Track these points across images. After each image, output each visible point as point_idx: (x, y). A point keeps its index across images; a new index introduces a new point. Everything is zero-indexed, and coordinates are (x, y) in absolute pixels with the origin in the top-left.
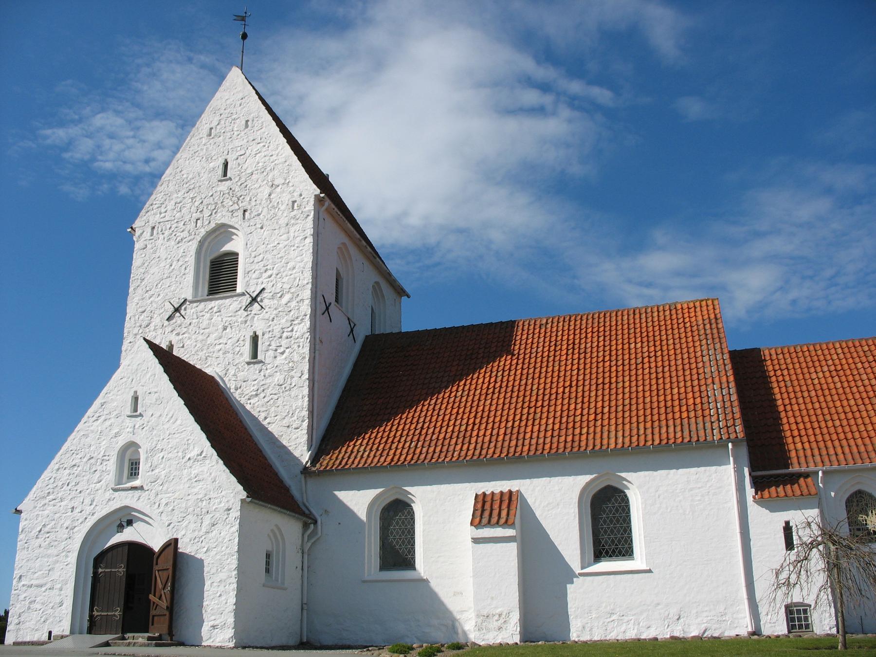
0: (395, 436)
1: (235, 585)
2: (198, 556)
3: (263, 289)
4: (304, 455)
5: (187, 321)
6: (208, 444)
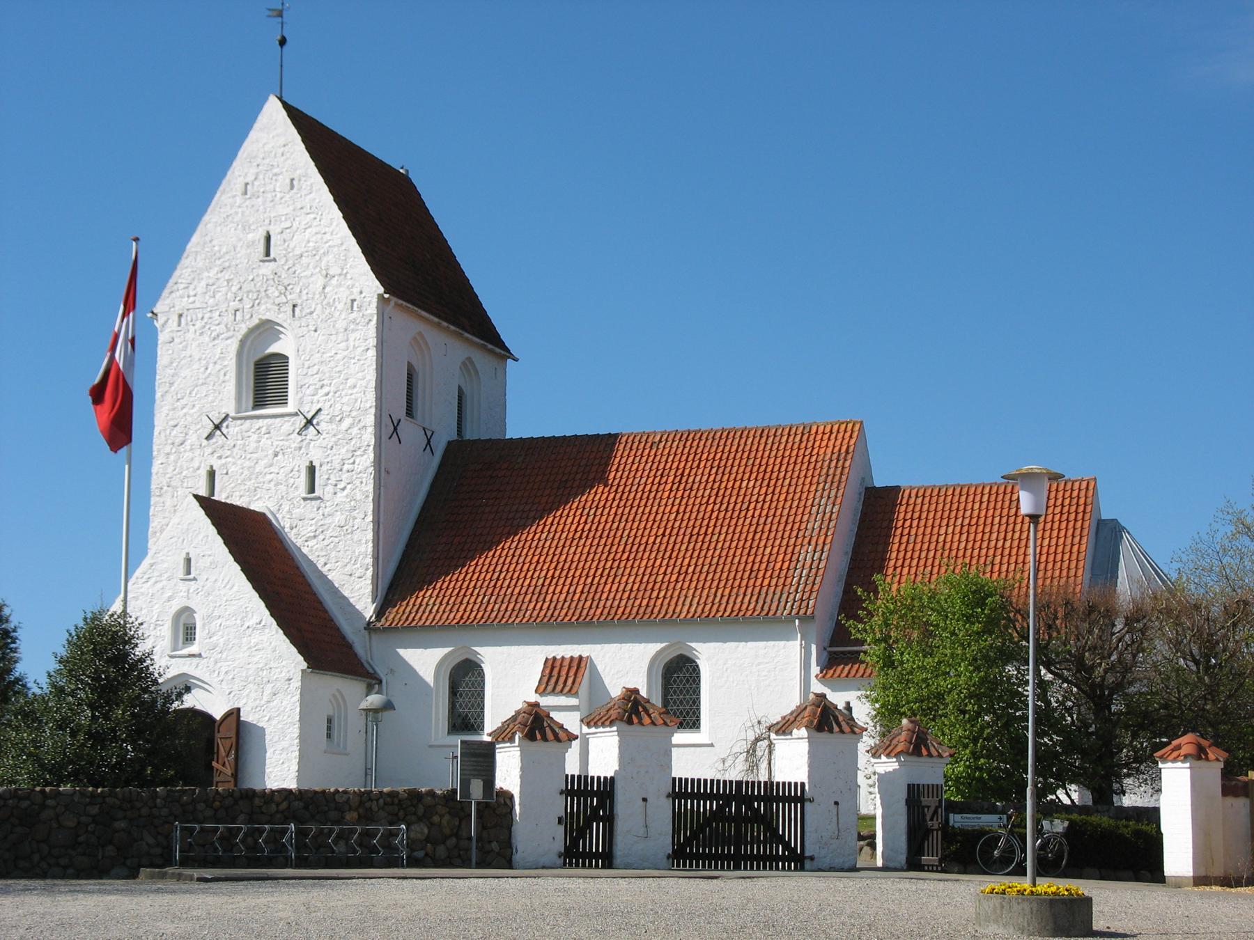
0: (468, 588)
1: (297, 753)
2: (260, 725)
3: (320, 410)
4: (368, 609)
5: (231, 442)
6: (268, 613)
